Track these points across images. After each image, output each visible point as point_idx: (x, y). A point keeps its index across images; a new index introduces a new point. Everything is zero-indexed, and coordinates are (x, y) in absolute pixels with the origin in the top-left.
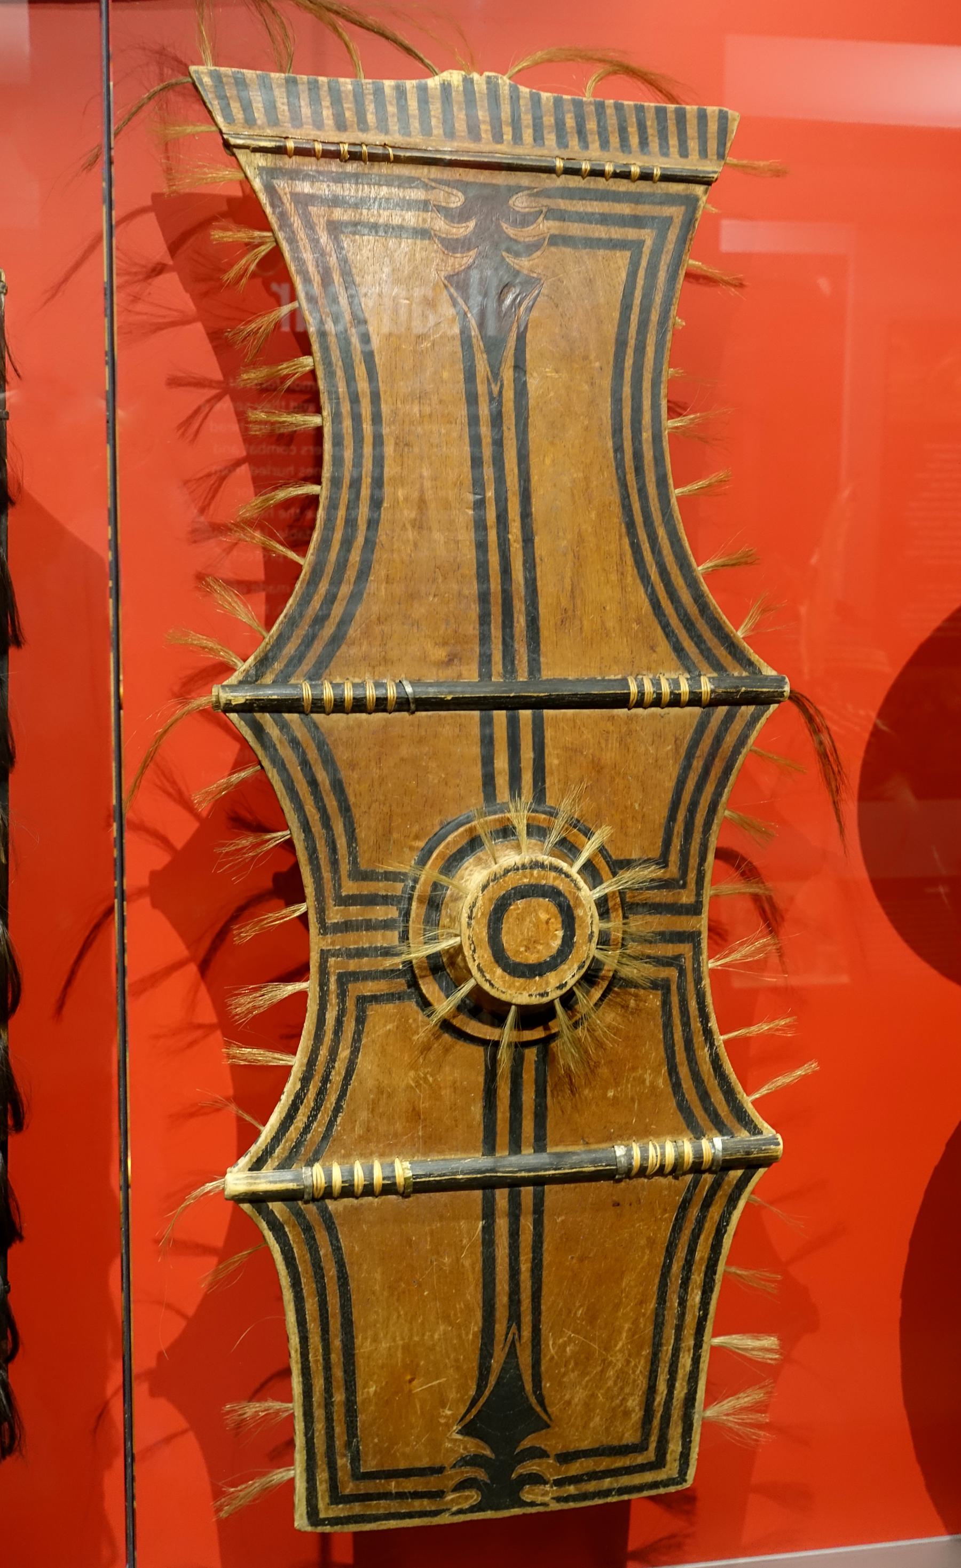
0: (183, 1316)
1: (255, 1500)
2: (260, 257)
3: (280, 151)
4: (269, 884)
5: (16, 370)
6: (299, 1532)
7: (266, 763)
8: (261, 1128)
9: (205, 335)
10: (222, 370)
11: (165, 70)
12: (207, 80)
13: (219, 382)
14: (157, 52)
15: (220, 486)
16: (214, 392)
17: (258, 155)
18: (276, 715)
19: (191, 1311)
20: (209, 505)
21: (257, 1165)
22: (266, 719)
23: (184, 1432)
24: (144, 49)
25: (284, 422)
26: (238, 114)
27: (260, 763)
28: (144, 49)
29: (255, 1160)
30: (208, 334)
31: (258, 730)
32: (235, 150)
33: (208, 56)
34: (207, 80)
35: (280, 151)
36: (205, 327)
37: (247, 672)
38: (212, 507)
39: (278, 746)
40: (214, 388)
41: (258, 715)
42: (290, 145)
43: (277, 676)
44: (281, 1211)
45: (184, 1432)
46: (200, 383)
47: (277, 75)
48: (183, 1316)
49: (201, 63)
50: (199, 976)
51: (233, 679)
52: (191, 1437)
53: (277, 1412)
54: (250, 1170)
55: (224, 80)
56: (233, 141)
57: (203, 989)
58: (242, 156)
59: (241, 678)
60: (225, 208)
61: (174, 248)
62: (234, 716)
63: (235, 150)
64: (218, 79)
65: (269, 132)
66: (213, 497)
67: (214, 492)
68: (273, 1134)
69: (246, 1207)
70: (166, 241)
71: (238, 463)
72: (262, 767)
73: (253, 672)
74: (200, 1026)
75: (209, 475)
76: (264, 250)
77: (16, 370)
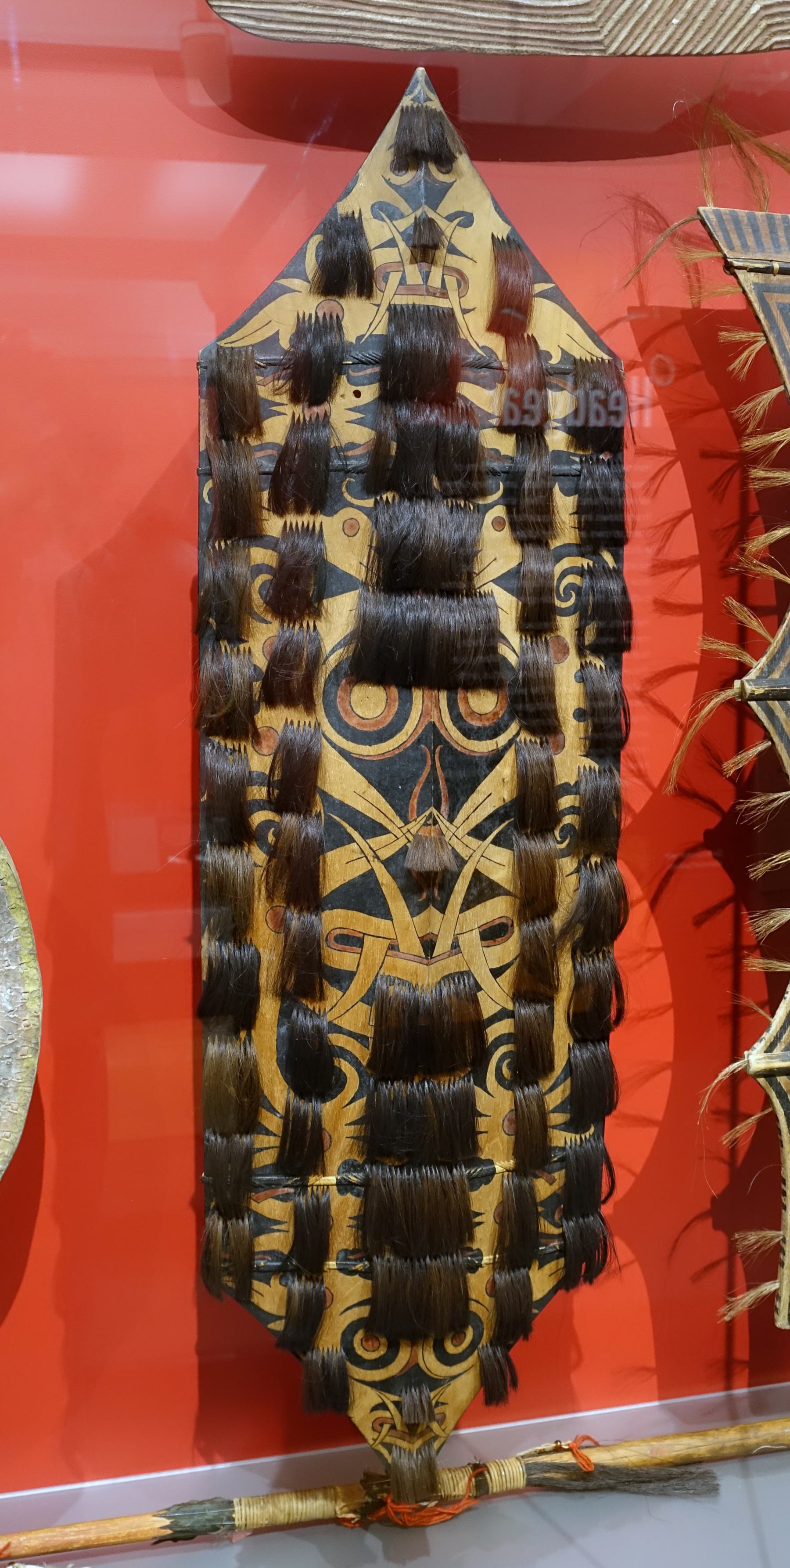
0: (633, 1174)
1: (751, 1306)
2: (756, 351)
3: (768, 271)
4: (700, 838)
5: (633, 437)
6: (780, 1330)
7: (776, 739)
8: (772, 1020)
9: (664, 416)
10: (676, 443)
11: (639, 212)
12: (712, 217)
13: (673, 451)
14: (633, 198)
15: (672, 531)
16: (669, 459)
17: (752, 274)
18: (782, 702)
19: (638, 1169)
20: (664, 546)
21: (770, 1048)
22: (776, 705)
23: (632, 1262)
24: (624, 196)
25: (778, 478)
26: (736, 242)
27: (771, 740)
28: (624, 196)
29: (768, 1044)
30: (666, 414)
31: (771, 714)
32: (737, 271)
33: (710, 200)
34: (712, 217)
35: (768, 271)
36: (664, 409)
37: (762, 669)
38: (667, 546)
39: (784, 726)
40: (670, 456)
41: (770, 702)
42: (776, 266)
43: (782, 672)
44: (786, 1084)
45: (632, 1262)
46: (659, 453)
47: (760, 213)
48: (633, 1174)
49: (705, 205)
50: (649, 910)
51: (753, 674)
52: (636, 1264)
53: (772, 1238)
54: (765, 1052)
55: (724, 217)
56: (736, 263)
57: (652, 920)
58: (741, 274)
59: (758, 674)
60: (679, 317)
61: (643, 349)
62: (753, 704)
63: (737, 271)
64: (719, 216)
65: (759, 256)
66: (668, 539)
67: (668, 536)
68: (781, 1024)
69: (762, 1081)
70: (637, 343)
71: (685, 514)
72: (773, 743)
73: (766, 669)
74: (649, 950)
75: (664, 523)
76: (758, 346)
77: (633, 437)
